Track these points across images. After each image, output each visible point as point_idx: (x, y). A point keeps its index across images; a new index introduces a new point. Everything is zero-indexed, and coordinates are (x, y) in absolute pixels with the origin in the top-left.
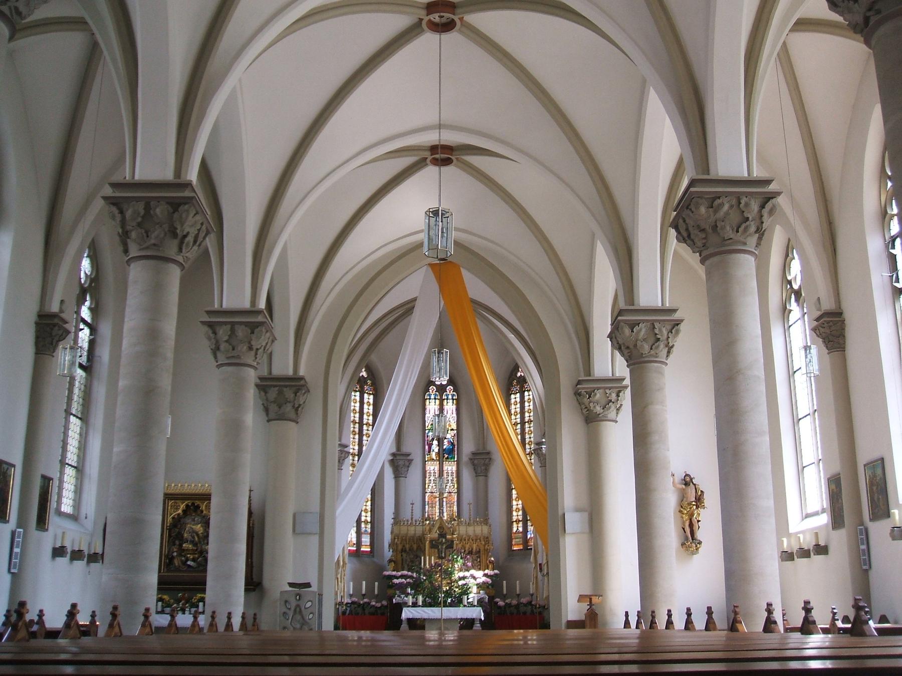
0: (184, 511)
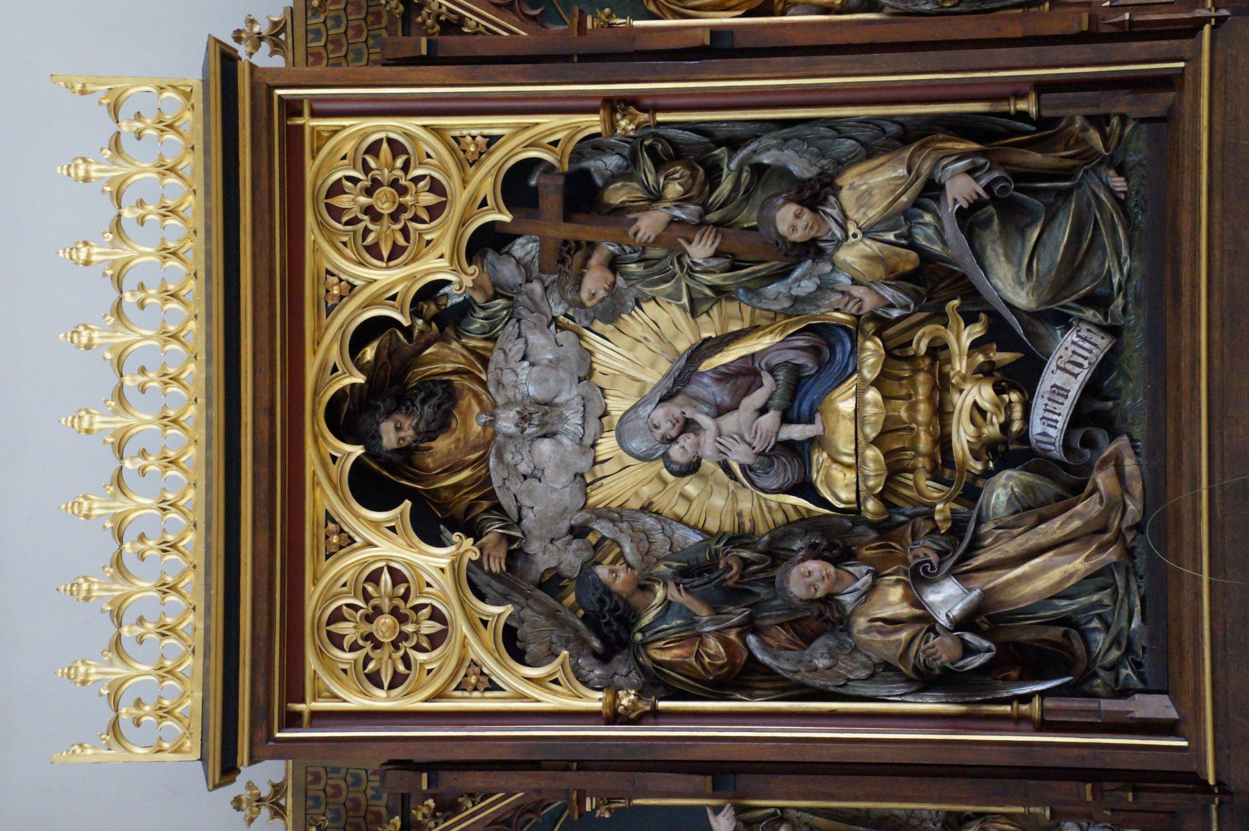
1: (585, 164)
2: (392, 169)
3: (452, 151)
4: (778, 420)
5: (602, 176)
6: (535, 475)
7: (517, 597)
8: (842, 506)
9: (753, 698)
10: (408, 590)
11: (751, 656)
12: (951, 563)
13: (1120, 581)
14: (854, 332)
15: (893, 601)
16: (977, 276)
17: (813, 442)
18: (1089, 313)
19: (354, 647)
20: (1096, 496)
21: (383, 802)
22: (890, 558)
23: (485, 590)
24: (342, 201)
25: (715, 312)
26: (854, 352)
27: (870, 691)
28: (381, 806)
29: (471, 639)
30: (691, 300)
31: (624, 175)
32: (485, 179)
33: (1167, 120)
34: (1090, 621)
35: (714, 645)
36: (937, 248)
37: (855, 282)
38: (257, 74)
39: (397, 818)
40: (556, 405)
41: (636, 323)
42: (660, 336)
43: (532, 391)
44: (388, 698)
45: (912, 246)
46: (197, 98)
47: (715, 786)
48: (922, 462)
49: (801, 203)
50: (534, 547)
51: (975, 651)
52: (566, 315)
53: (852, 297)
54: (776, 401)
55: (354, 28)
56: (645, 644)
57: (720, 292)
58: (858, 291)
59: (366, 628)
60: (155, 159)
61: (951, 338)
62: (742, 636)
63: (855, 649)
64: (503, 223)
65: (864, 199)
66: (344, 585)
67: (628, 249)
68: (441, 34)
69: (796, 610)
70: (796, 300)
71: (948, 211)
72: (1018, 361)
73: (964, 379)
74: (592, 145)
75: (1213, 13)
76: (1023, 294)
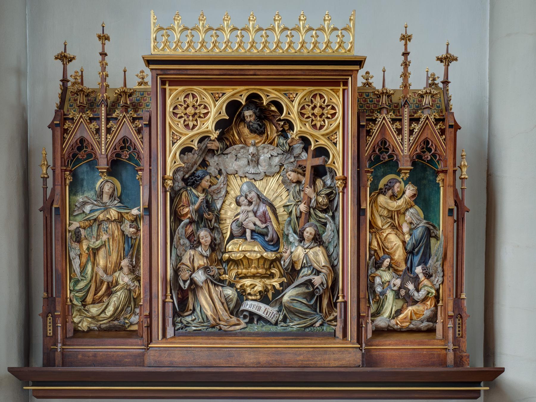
0: (220, 125)
1: (328, 173)
2: (327, 113)
3: (332, 132)
4: (252, 229)
5: (325, 179)
7: (201, 153)
8: (227, 247)
12: (210, 278)
17: (246, 239)
18: (281, 317)
20: (229, 318)
30: (288, 206)
31: (325, 184)
32: (323, 142)
34: (194, 316)
35: (186, 210)
36: (301, 275)
38: (355, 72)
39: (136, 116)
40: (258, 165)
43: (262, 158)
44: (170, 112)
45: (302, 268)
49: (315, 235)
50: (216, 158)
51: (184, 284)
52: (284, 169)
55: (369, 106)
56: (187, 190)
59: (191, 105)
61: (276, 279)
62: (189, 218)
63: (186, 251)
65: (316, 254)
66: (203, 99)
67: (303, 186)
68: (367, 130)
70: (288, 235)
73: (263, 282)
75: (363, 348)
76: (287, 298)
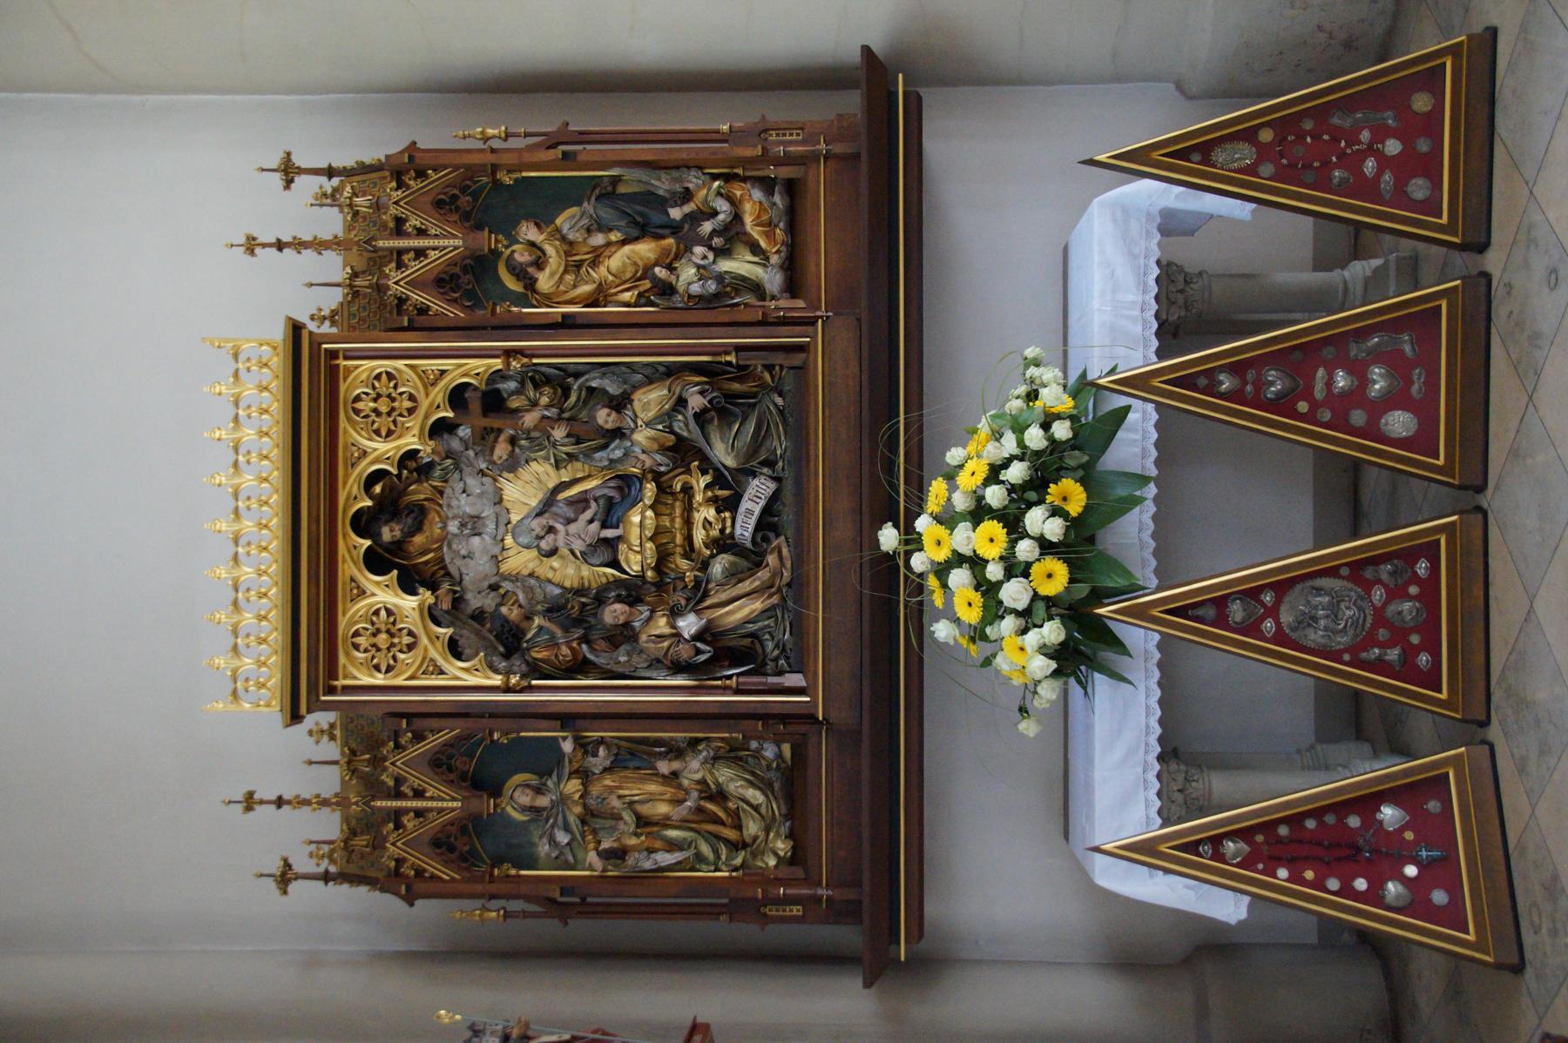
2: (388, 388)
3: (420, 378)
6: (469, 556)
9: (587, 678)
10: (395, 620)
11: (585, 657)
13: (779, 615)
14: (641, 479)
15: (661, 625)
16: (707, 449)
17: (619, 538)
18: (765, 470)
19: (366, 651)
20: (768, 569)
21: (386, 734)
22: (662, 602)
23: (441, 619)
24: (360, 405)
25: (569, 467)
26: (641, 490)
27: (648, 674)
28: (385, 735)
29: (430, 647)
30: (556, 461)
31: (517, 392)
32: (439, 393)
33: (802, 370)
35: (565, 650)
36: (685, 434)
37: (644, 452)
40: (483, 518)
41: (527, 473)
42: (539, 480)
43: (468, 510)
44: (385, 679)
45: (672, 432)
46: (280, 349)
47: (562, 727)
48: (679, 550)
50: (469, 596)
53: (639, 460)
54: (599, 516)
56: (528, 649)
57: (571, 457)
58: (643, 457)
60: (257, 382)
61: (694, 482)
62: (579, 644)
64: (449, 418)
65: (646, 407)
68: (417, 315)
69: (609, 630)
70: (611, 461)
71: (690, 413)
72: (731, 495)
73: (700, 504)
74: (498, 375)
76: (729, 459)
